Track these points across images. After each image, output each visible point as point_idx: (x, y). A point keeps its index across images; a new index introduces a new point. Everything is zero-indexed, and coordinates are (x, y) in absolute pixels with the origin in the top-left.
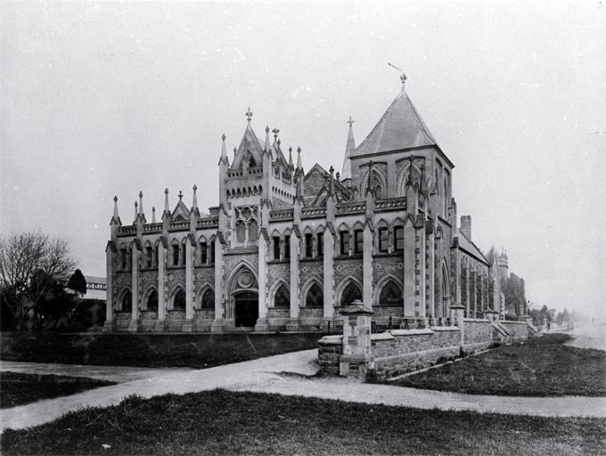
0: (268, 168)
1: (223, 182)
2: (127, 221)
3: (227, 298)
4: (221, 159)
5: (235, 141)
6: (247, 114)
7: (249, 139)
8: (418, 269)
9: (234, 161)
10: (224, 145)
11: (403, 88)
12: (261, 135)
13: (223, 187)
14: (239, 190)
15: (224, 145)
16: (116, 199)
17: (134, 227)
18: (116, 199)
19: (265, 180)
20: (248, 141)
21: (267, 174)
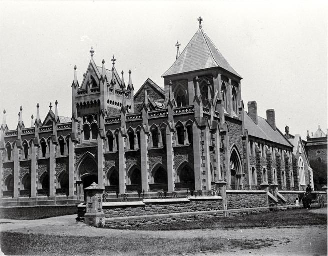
0: (104, 88)
1: (74, 99)
2: (13, 127)
3: (78, 180)
4: (19, 124)
5: (83, 70)
6: (91, 52)
7: (91, 68)
8: (204, 156)
9: (83, 83)
10: (38, 111)
11: (201, 27)
12: (99, 64)
13: (75, 102)
14: (114, 102)
15: (38, 111)
16: (38, 106)
17: (16, 132)
18: (38, 106)
19: (102, 96)
20: (92, 69)
21: (104, 92)
